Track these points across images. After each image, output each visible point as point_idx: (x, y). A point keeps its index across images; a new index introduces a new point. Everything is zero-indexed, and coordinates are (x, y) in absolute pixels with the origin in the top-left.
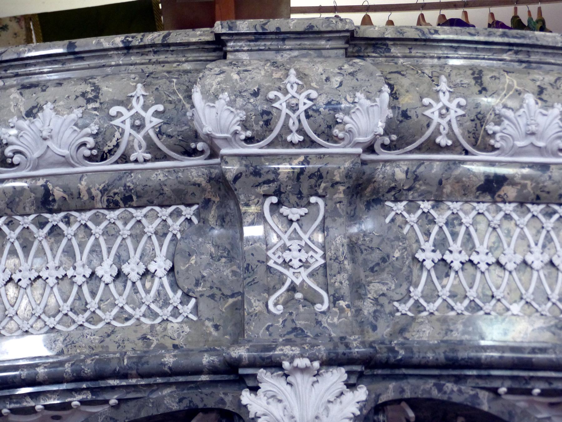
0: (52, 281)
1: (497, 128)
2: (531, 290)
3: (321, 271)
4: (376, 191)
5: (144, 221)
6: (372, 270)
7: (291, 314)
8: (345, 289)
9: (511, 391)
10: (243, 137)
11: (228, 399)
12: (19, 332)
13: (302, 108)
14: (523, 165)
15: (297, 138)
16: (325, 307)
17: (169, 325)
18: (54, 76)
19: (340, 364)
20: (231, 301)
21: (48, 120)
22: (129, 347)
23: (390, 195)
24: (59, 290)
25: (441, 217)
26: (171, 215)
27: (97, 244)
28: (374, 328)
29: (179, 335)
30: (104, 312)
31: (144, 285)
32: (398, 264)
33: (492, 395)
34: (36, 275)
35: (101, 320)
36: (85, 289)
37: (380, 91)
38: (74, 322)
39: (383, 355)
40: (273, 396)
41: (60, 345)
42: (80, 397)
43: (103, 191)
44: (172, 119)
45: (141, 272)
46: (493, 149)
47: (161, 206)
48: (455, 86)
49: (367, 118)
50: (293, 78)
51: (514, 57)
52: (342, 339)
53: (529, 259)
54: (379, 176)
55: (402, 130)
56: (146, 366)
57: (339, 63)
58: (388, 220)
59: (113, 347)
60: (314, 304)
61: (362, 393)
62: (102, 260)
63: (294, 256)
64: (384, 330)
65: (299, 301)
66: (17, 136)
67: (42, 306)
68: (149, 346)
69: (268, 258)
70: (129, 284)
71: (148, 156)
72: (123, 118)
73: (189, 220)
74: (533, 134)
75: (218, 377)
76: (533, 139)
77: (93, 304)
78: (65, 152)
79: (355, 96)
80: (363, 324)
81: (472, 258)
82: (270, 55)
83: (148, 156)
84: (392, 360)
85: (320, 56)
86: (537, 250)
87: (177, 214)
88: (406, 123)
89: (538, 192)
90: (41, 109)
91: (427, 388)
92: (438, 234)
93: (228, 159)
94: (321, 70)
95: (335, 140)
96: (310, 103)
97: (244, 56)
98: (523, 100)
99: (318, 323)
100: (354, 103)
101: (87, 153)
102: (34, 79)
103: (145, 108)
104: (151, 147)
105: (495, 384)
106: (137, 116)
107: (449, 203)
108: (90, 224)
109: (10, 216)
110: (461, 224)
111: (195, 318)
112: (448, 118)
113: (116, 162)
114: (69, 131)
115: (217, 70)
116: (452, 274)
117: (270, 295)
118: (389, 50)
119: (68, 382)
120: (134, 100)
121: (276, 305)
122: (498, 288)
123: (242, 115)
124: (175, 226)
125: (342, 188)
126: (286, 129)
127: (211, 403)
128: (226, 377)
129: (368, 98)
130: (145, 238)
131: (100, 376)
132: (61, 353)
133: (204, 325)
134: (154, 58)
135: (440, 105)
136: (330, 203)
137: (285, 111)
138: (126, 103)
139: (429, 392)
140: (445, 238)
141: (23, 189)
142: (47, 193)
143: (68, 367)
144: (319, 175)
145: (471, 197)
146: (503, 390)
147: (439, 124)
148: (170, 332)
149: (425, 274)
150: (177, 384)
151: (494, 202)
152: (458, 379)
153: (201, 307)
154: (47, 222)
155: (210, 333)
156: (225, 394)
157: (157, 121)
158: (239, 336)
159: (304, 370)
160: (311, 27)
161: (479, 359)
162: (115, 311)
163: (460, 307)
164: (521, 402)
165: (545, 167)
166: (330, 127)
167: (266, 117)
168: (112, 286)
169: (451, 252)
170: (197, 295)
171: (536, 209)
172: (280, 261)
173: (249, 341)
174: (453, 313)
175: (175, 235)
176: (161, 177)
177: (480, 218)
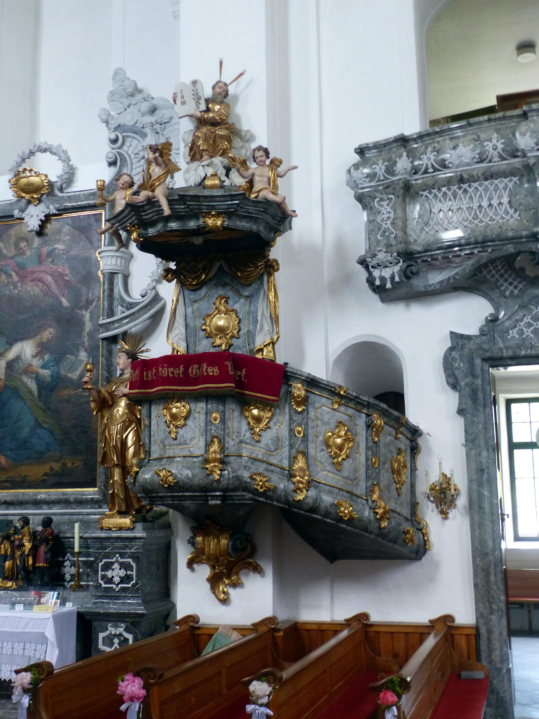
0: (465, 209)
20: (533, 211)
21: (462, 150)
22: (494, 231)
27: (481, 194)
36: (478, 211)
41: (469, 232)
43: (483, 174)
59: (489, 231)
70: (494, 208)
71: (499, 159)
72: (489, 146)
73: (516, 183)
77: (480, 216)
97: (535, 118)
101: (476, 160)
103: (497, 141)
106: (495, 145)
113: (487, 163)
119: (473, 244)
124: (510, 185)
127: (526, 249)
130: (499, 191)
131: (484, 242)
132: (470, 234)
134: (500, 122)
138: (490, 140)
143: (472, 240)
150: (514, 243)
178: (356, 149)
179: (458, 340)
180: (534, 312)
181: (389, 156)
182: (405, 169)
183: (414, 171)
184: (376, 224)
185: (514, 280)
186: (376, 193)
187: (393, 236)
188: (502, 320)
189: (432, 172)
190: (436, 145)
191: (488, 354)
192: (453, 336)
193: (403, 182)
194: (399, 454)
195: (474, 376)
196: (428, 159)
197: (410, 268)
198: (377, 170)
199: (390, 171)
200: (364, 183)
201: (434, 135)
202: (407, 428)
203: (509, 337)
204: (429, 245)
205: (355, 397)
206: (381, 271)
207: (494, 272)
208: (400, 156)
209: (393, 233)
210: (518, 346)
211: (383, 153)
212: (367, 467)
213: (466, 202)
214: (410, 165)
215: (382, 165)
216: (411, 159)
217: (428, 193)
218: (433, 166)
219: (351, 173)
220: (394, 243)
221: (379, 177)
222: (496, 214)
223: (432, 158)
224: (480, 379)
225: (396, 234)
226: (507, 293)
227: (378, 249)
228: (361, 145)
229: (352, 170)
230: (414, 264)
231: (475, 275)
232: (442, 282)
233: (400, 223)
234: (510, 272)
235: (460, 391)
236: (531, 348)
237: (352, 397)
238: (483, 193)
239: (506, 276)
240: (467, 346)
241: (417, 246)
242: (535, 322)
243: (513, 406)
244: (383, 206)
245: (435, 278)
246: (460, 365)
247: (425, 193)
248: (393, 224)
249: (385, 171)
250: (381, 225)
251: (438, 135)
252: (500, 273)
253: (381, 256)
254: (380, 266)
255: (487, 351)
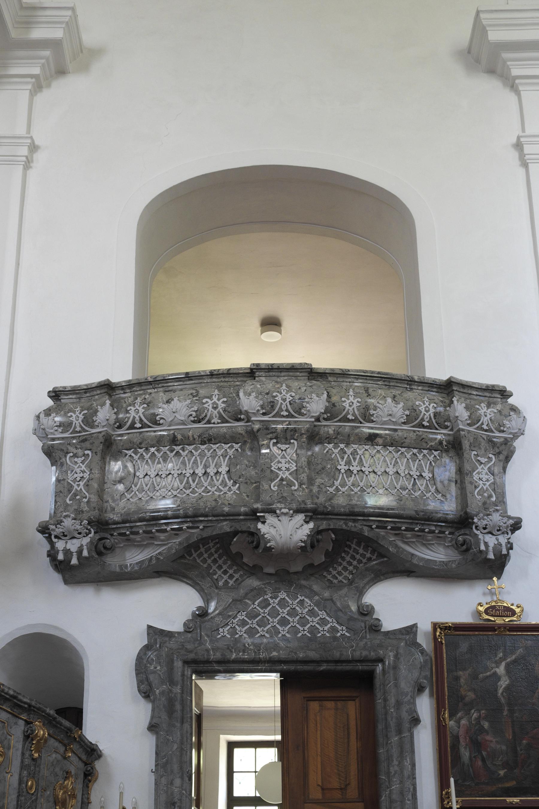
0: (176, 475)
1: (374, 412)
2: (388, 484)
3: (295, 473)
4: (320, 439)
5: (217, 450)
6: (318, 473)
7: (281, 490)
8: (305, 480)
9: (378, 527)
10: (261, 412)
11: (252, 526)
12: (161, 497)
13: (288, 400)
14: (386, 429)
15: (285, 413)
16: (296, 488)
17: (227, 495)
18: (179, 387)
19: (302, 512)
20: (254, 485)
21: (176, 404)
22: (209, 504)
23: (326, 441)
24: (179, 479)
25: (349, 451)
26: (229, 447)
27: (196, 460)
28: (318, 498)
29: (231, 499)
30: (198, 489)
31: (216, 478)
32: (329, 471)
33: (369, 529)
34: (169, 472)
35: (197, 492)
36: (190, 479)
37: (323, 394)
38: (185, 493)
39: (321, 509)
40: (272, 526)
41: (178, 502)
42: (187, 525)
43: (199, 436)
44: (230, 404)
45: (215, 472)
46: (373, 421)
47: (225, 443)
48: (357, 393)
49: (317, 405)
50: (284, 387)
51: (383, 383)
52: (303, 501)
53: (388, 470)
54: (322, 432)
55: (332, 412)
56: (216, 511)
57: (305, 382)
58: (325, 452)
59: (202, 504)
60: (291, 486)
61: (311, 525)
62: (198, 467)
63: (283, 466)
64: (322, 499)
65: (284, 485)
66: (162, 412)
67: (171, 486)
68: (218, 503)
69: (271, 466)
70: (210, 477)
71: (219, 421)
72: (209, 404)
73: (237, 450)
74: (390, 415)
75: (248, 517)
76: (390, 417)
77: (193, 485)
78: (183, 418)
79: (312, 396)
80: (312, 496)
81: (362, 469)
82: (275, 378)
83: (219, 421)
84: (325, 511)
85: (297, 379)
86: (391, 467)
87: (232, 447)
88: (334, 409)
89: (392, 441)
90: (173, 400)
91: (341, 524)
92: (347, 458)
93: (254, 422)
94: (297, 385)
95: (303, 415)
96: (291, 398)
97: (263, 379)
98: (386, 400)
99: (293, 494)
100: (311, 398)
101: (192, 419)
102: (170, 388)
103: (219, 400)
104: (221, 417)
105: (370, 524)
106: (214, 403)
107: (353, 445)
108: (193, 451)
109: (158, 447)
110: (358, 454)
111: (238, 492)
112: (353, 407)
113: (205, 424)
114: (185, 409)
115: (251, 383)
116: (353, 476)
117: (272, 482)
118: (328, 378)
119: (181, 518)
120: (214, 396)
121: (274, 486)
122: (373, 482)
123: (261, 402)
124: (231, 452)
125: (305, 436)
126: (281, 409)
127: (244, 529)
128: (251, 517)
129: (317, 397)
130: (217, 457)
131: (195, 516)
132: (179, 506)
133: (242, 495)
134: (223, 380)
135: (350, 401)
136: (299, 442)
137: (280, 401)
138: (210, 397)
139: (341, 526)
140: (350, 460)
141: (164, 435)
142: (175, 437)
143: (181, 512)
144: (295, 430)
145: (362, 443)
146: (374, 526)
147: (349, 410)
148: (227, 498)
149: (341, 475)
150: (229, 520)
151: (373, 445)
152: (355, 521)
153: (241, 487)
154: (174, 450)
155: (245, 499)
156: (251, 524)
157: (223, 405)
158: (258, 499)
159: (285, 514)
160: (293, 366)
161: (364, 512)
162: (203, 488)
163: (356, 490)
164: (382, 532)
165: (395, 430)
166: (300, 409)
167: (272, 404)
168: (202, 478)
169: (353, 466)
170: (240, 482)
171: (391, 449)
172: (277, 468)
173: (262, 501)
174: (353, 493)
175: (230, 456)
176: (225, 430)
177: (366, 452)
178: (49, 392)
179: (157, 636)
180: (251, 608)
181: (90, 403)
182: (107, 420)
183: (118, 424)
184: (66, 484)
185: (230, 567)
186: (69, 447)
187: (85, 500)
188: (212, 615)
189: (140, 428)
190: (147, 396)
191: (191, 656)
192: (151, 631)
193: (104, 436)
194: (66, 778)
195: (172, 682)
196: (136, 412)
197: (103, 541)
198: (73, 419)
199: (89, 421)
200: (56, 433)
201: (145, 385)
202: (82, 747)
203: (219, 637)
204: (128, 514)
205: (11, 696)
206: (66, 542)
207: (206, 556)
208: (103, 405)
209: (86, 498)
210: (229, 648)
211: (83, 400)
212: (19, 792)
213: (178, 467)
214: (114, 417)
215: (80, 413)
216: (116, 410)
217: (133, 452)
218: (141, 420)
219: (41, 419)
220: (86, 508)
221: (75, 427)
222: (212, 485)
223: (141, 410)
224: (179, 687)
225: (90, 498)
226: (221, 584)
227: (64, 514)
228: (57, 388)
229: (42, 416)
230: (109, 537)
231: (183, 557)
232: (142, 562)
233: (96, 486)
234: (225, 557)
235: (153, 702)
236: (244, 651)
237: (8, 696)
238: (198, 458)
239: (220, 562)
240: (167, 644)
241: (114, 514)
242: (250, 620)
243: (237, 752)
244: (76, 463)
245: (134, 557)
246: (158, 668)
247: (130, 452)
248: (87, 485)
249: (82, 421)
250: (72, 486)
251: (151, 387)
252: (213, 558)
253: (68, 523)
254: (66, 536)
255: (191, 652)
